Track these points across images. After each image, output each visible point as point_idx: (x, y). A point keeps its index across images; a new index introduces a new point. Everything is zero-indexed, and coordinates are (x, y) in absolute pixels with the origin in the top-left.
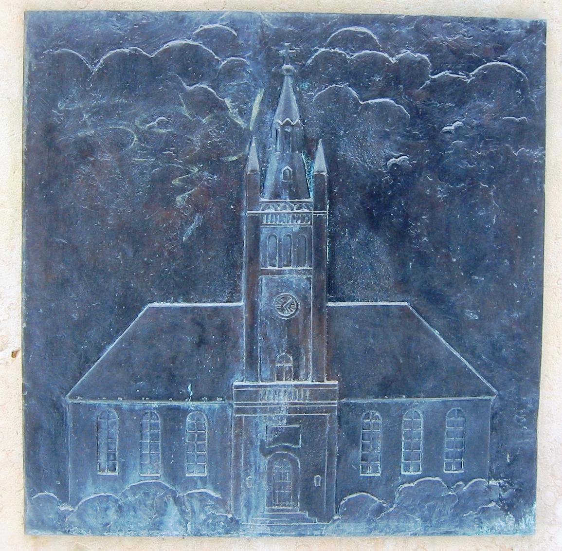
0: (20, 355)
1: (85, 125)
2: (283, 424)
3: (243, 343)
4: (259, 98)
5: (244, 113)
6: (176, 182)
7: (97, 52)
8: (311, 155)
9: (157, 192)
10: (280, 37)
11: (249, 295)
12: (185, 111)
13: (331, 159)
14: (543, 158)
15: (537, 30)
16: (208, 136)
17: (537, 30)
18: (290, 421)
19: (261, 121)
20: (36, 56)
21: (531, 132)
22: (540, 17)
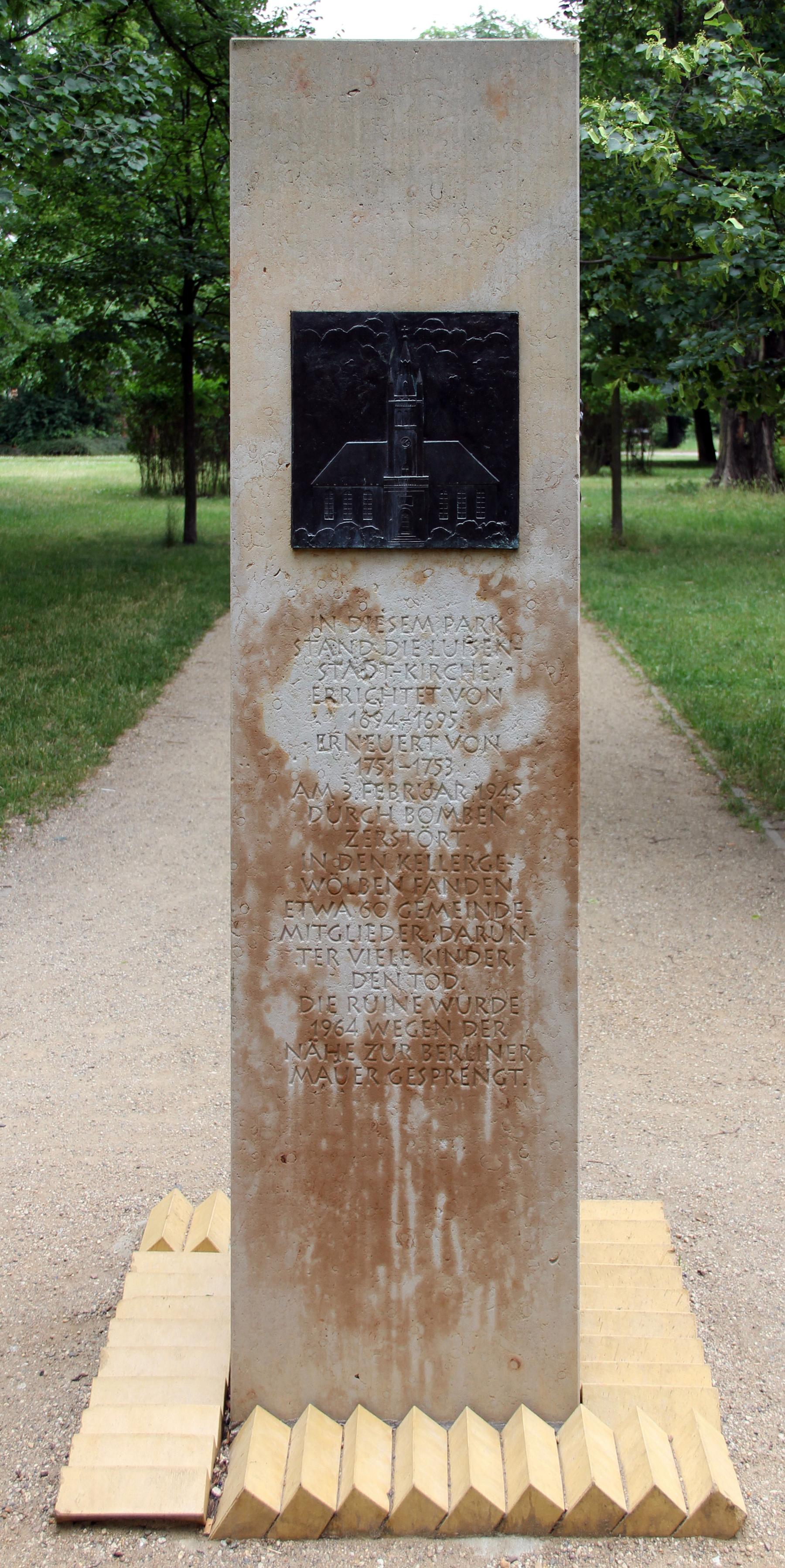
0: (290, 466)
1: (318, 364)
2: (405, 495)
3: (387, 459)
4: (393, 351)
5: (387, 357)
6: (358, 388)
7: (322, 331)
8: (416, 376)
9: (678, 205)
10: (401, 323)
11: (462, 550)
12: (362, 357)
13: (424, 376)
14: (517, 375)
15: (514, 318)
16: (371, 368)
17: (514, 318)
18: (408, 494)
19: (394, 361)
20: (297, 332)
21: (170, 421)
22: (517, 309)
